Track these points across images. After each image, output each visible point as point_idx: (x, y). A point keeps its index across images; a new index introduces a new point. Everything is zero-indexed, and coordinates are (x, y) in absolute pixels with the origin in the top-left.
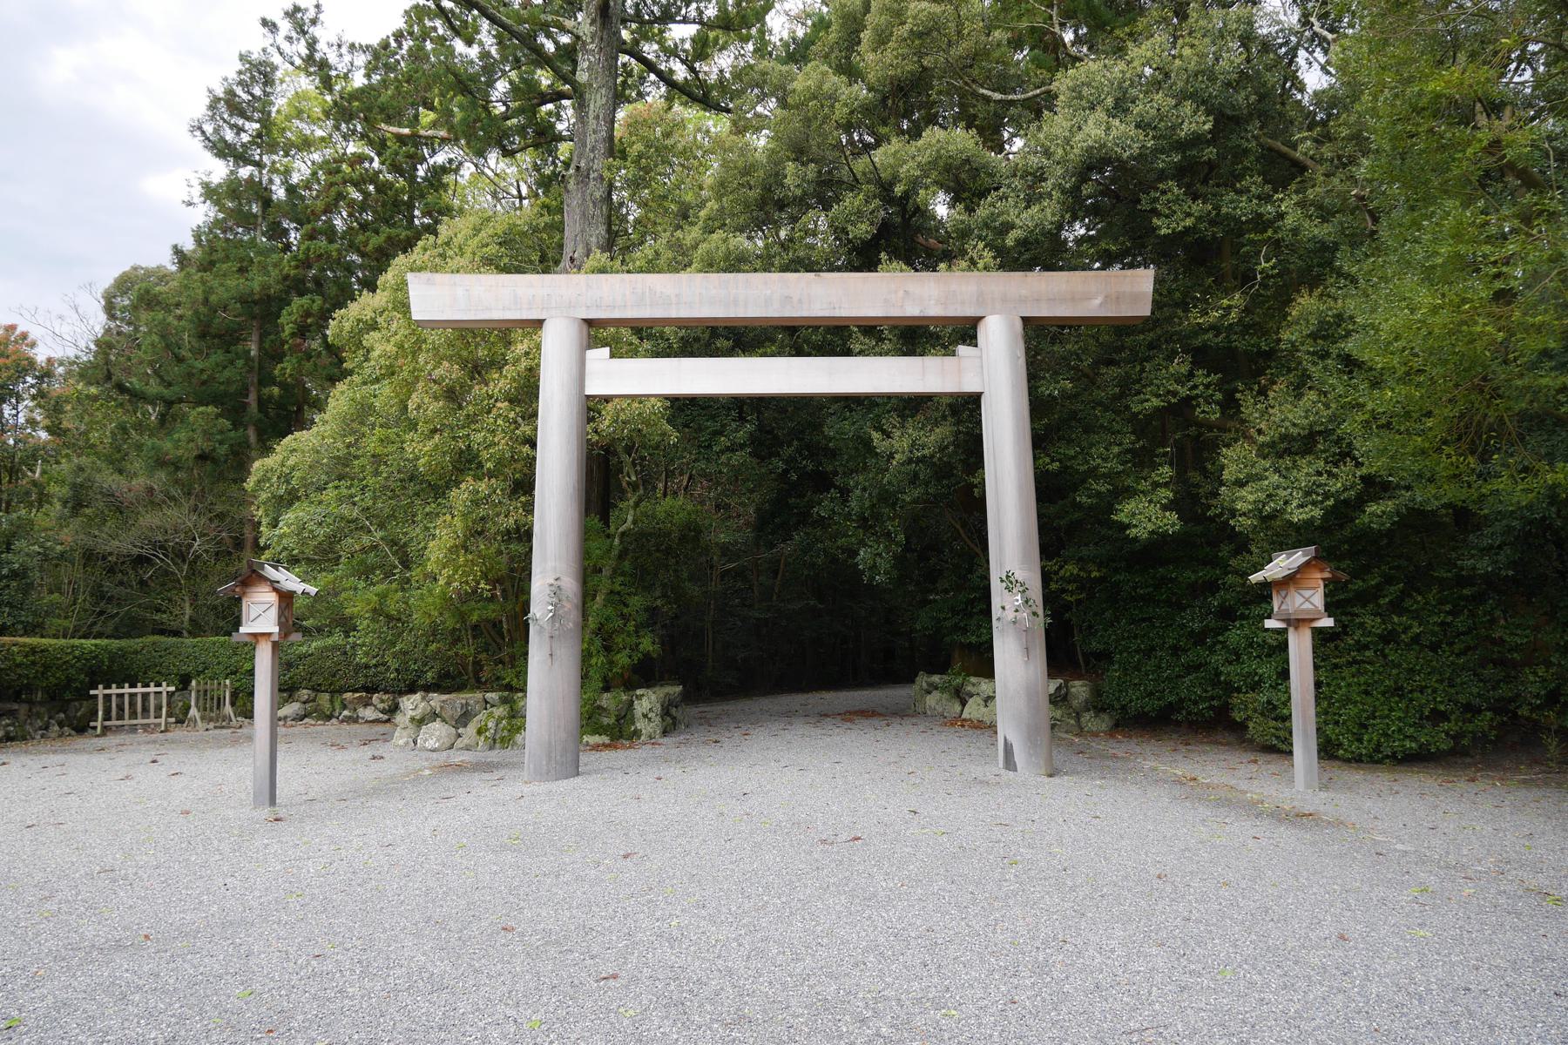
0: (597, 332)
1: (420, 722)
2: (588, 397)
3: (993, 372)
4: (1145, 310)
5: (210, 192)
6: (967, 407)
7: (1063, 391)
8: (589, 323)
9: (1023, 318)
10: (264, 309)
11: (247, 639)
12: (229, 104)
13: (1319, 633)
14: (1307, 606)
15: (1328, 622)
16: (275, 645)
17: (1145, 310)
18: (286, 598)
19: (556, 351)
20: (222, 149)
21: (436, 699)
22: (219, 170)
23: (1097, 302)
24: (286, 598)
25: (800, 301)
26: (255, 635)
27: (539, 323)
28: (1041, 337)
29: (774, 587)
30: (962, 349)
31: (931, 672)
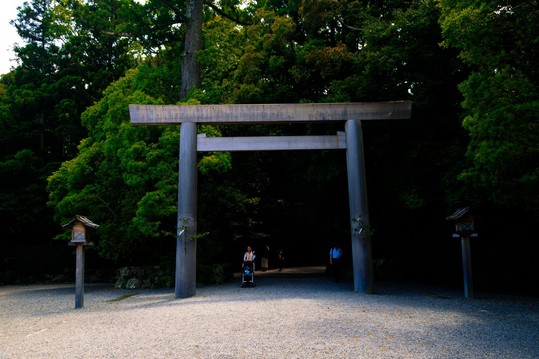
0: (199, 127)
1: (127, 278)
2: (198, 152)
3: (349, 140)
4: (409, 117)
5: (21, 52)
6: (341, 154)
8: (197, 124)
9: (362, 121)
10: (46, 105)
11: (73, 245)
12: (28, 14)
13: (472, 239)
14: (468, 229)
15: (475, 235)
16: (84, 247)
17: (409, 117)
18: (88, 229)
19: (185, 134)
20: (24, 34)
21: (134, 270)
22: (23, 43)
23: (390, 114)
24: (88, 229)
25: (278, 115)
26: (76, 243)
27: (180, 124)
28: (367, 128)
29: (261, 230)
30: (339, 133)
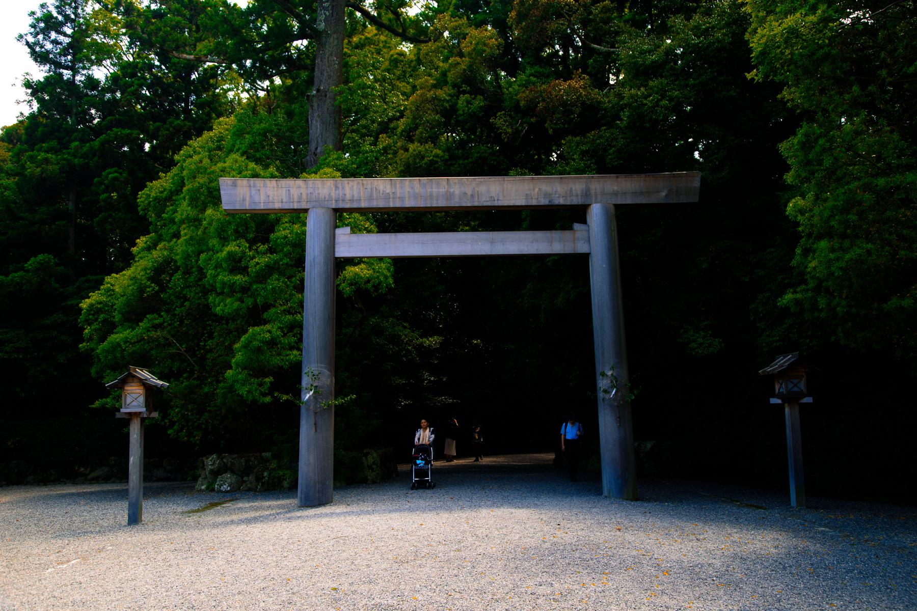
0: (339, 216)
1: (216, 473)
2: (337, 258)
4: (695, 199)
5: (35, 89)
6: (580, 262)
7: (847, 16)
8: (336, 210)
9: (615, 205)
10: (78, 178)
11: (124, 416)
12: (47, 23)
13: (803, 407)
14: (796, 389)
15: (808, 400)
16: (143, 420)
17: (695, 199)
18: (150, 390)
19: (315, 228)
20: (40, 57)
21: (228, 459)
22: (39, 73)
23: (664, 194)
24: (150, 390)
25: (472, 196)
26: (130, 414)
27: (306, 211)
28: (625, 218)
30: (577, 226)
31: (254, 326)
